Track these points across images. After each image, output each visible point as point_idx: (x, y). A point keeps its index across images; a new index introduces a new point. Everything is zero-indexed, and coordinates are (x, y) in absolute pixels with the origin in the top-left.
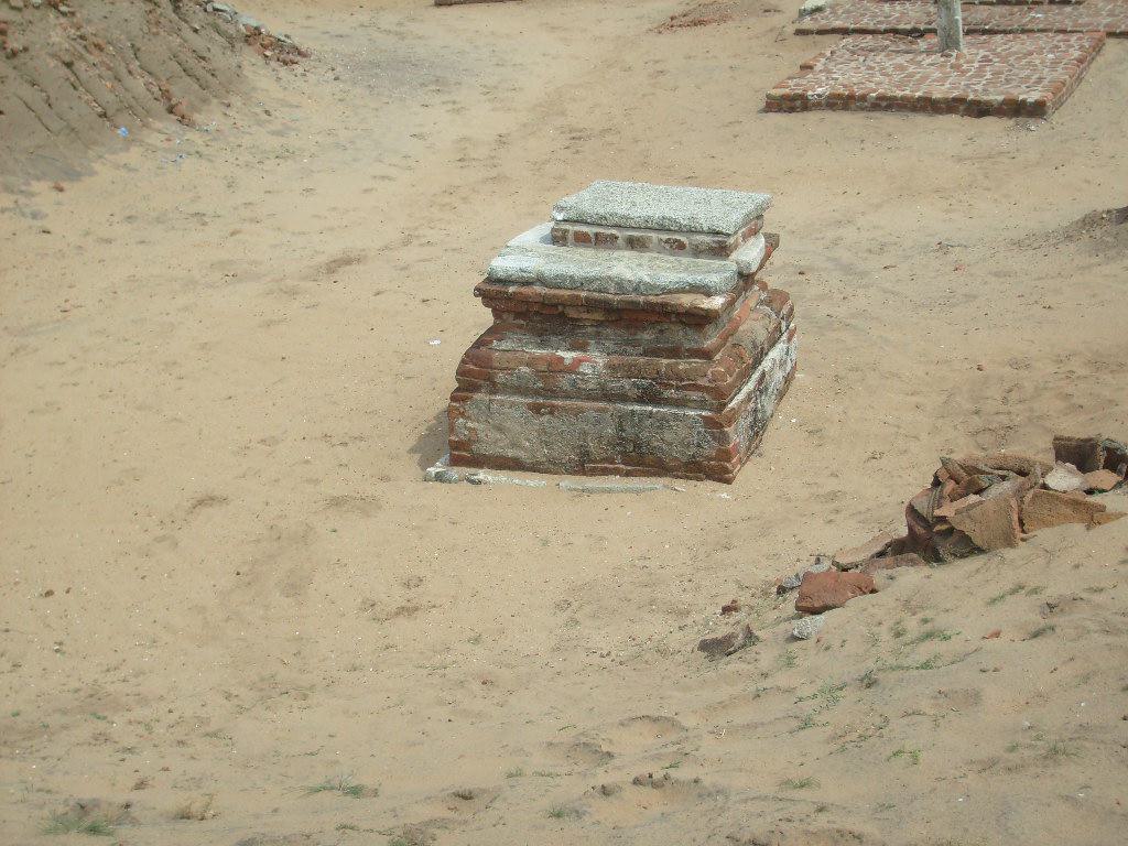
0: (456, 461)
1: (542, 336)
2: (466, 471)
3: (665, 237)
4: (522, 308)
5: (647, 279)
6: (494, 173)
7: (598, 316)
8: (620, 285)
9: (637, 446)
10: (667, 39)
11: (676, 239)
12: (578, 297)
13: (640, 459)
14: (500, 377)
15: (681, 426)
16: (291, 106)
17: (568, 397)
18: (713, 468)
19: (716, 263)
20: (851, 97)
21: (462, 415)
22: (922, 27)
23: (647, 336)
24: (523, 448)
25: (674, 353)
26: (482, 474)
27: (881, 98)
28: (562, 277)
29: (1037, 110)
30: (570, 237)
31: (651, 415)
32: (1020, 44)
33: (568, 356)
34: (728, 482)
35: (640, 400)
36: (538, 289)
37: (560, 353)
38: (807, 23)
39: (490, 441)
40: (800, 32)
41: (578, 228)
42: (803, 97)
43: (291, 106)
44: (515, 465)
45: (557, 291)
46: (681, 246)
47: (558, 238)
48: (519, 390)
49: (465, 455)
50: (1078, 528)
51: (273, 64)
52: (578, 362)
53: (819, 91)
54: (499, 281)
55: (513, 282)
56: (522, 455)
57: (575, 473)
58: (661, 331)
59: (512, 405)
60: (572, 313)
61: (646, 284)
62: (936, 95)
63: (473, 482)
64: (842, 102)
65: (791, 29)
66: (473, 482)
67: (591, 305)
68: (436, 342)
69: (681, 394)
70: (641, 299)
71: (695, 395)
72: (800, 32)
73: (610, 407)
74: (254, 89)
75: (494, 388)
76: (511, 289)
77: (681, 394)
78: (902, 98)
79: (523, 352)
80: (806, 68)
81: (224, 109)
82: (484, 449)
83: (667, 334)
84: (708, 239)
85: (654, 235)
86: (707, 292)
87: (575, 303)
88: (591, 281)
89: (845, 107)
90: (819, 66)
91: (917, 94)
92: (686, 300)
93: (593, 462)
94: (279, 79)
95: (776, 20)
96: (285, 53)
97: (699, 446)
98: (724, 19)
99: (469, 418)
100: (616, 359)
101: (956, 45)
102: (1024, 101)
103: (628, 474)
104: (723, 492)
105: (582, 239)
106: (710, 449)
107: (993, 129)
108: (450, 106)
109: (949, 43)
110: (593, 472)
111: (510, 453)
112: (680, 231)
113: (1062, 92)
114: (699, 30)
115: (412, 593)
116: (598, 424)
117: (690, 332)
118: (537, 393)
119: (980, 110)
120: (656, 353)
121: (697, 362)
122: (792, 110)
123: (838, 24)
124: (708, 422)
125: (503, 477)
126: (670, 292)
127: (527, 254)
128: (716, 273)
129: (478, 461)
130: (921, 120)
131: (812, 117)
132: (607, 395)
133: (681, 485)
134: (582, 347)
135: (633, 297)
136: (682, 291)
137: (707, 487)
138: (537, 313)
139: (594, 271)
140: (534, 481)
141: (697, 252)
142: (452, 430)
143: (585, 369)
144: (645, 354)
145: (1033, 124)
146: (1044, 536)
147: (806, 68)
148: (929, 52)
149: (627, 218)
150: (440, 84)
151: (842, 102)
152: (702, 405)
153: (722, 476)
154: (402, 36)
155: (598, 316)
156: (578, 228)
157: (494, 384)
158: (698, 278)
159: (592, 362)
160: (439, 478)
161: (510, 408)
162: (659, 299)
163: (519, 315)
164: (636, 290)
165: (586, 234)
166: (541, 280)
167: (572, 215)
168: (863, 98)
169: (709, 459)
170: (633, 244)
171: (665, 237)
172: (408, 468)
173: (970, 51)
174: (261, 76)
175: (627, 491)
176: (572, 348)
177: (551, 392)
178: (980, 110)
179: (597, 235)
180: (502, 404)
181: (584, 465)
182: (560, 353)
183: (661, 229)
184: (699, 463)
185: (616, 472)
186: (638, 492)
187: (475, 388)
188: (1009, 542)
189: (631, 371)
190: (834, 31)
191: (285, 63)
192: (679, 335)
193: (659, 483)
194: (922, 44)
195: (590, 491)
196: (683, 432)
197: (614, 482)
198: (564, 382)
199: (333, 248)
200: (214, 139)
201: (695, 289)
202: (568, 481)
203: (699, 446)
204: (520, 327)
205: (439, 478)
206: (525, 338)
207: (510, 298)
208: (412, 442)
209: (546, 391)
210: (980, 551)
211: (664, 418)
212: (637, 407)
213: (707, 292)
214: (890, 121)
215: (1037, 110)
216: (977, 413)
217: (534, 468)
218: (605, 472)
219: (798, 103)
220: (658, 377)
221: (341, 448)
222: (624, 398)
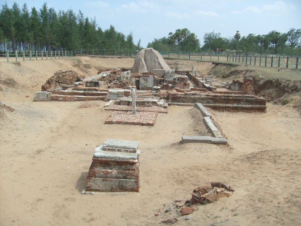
0: (87, 190)
1: (104, 167)
2: (90, 192)
3: (125, 149)
4: (97, 162)
5: (124, 157)
6: (59, 134)
7: (115, 164)
8: (119, 158)
9: (122, 186)
10: (80, 110)
11: (127, 150)
12: (112, 160)
13: (122, 189)
14: (97, 175)
15: (130, 182)
16: (15, 120)
17: (109, 178)
18: (135, 189)
19: (134, 154)
20: (120, 122)
21: (89, 182)
22: (127, 110)
23: (123, 167)
24: (101, 188)
25: (129, 170)
26: (93, 193)
27: (126, 122)
28: (109, 157)
29: (152, 125)
30: (107, 149)
31: (125, 181)
32: (145, 113)
33: (110, 171)
34: (138, 192)
35: (123, 178)
36: (104, 159)
37: (108, 170)
38: (106, 108)
39: (94, 187)
40: (105, 110)
41: (108, 148)
42: (112, 122)
43: (15, 120)
44: (99, 191)
45: (108, 159)
46: (127, 151)
47: (104, 149)
48: (100, 177)
49: (89, 189)
50: (226, 197)
51: (9, 111)
52: (112, 172)
53: (115, 121)
54: (97, 157)
55: (100, 158)
56: (100, 189)
57: (110, 192)
58: (126, 166)
59: (99, 180)
60: (110, 163)
61: (124, 158)
62: (135, 122)
63: (91, 194)
64: (119, 123)
65: (104, 109)
66: (91, 194)
67: (114, 162)
68: (69, 167)
69: (131, 177)
70: (123, 160)
71: (133, 177)
72: (105, 110)
73: (117, 179)
74: (7, 116)
75: (95, 177)
76: (99, 159)
77: (131, 177)
78: (129, 122)
79: (100, 170)
80: (110, 116)
81: (3, 120)
82: (92, 188)
83: (127, 167)
84: (132, 150)
85: (122, 149)
86: (134, 159)
87: (111, 161)
88: (114, 157)
89: (119, 124)
90: (112, 116)
91: (132, 122)
92: (131, 160)
93: (114, 189)
94: (11, 114)
95: (99, 107)
96: (11, 110)
97: (134, 186)
98: (90, 107)
99: (90, 182)
100: (119, 171)
101: (135, 113)
102: (150, 123)
103: (120, 191)
104: (138, 194)
105: (109, 150)
106: (135, 187)
107: (145, 127)
108: (45, 121)
109: (134, 113)
110: (114, 191)
111: (98, 188)
112: (127, 148)
113: (155, 121)
114: (86, 108)
115: (91, 216)
116: (115, 183)
117: (131, 166)
118: (104, 177)
119: (143, 125)
120: (126, 170)
121: (133, 171)
122: (110, 124)
123: (112, 109)
124: (135, 182)
125: (97, 193)
126: (128, 159)
127: (99, 153)
128: (134, 156)
129: (91, 190)
130: (133, 126)
131: (114, 125)
132: (117, 177)
133: (130, 193)
134: (112, 169)
135: (121, 160)
136: (130, 159)
137: (135, 193)
138: (104, 163)
139: (114, 156)
140: (103, 193)
141: (130, 152)
142: (87, 184)
143: (113, 173)
144: (123, 170)
145: (152, 127)
146: (221, 199)
147: (110, 116)
148: (130, 114)
149: (118, 146)
150: (42, 117)
151: (119, 123)
152: (134, 179)
153: (137, 191)
154: (31, 107)
155: (115, 164)
156: (108, 148)
157: (96, 176)
158: (133, 157)
159: (114, 172)
160: (85, 194)
161: (99, 181)
162: (127, 160)
163: (100, 163)
164: (122, 159)
165: (110, 149)
166: (105, 157)
167: (107, 145)
168: (123, 122)
169: (135, 188)
170: (118, 150)
171: (125, 149)
172: (76, 192)
173: (138, 114)
174: (7, 114)
175: (121, 194)
176: (110, 169)
177: (106, 177)
178: (143, 125)
179: (112, 149)
180: (97, 180)
181: (112, 190)
182: (108, 170)
183: (124, 148)
184: (133, 189)
185: (118, 191)
186: (123, 195)
187: (92, 177)
188: (216, 200)
189: (121, 173)
190: (111, 110)
191: (11, 111)
192: (129, 167)
193: (127, 193)
194: (128, 113)
195: (114, 195)
196: (131, 184)
197: (118, 193)
198: (109, 175)
199: (36, 148)
200: (3, 126)
201: (132, 159)
202: (109, 193)
203: (134, 186)
204: (100, 166)
205: (85, 194)
206: (101, 167)
207: (99, 160)
208: (75, 187)
209: (105, 177)
210: (212, 202)
211: (127, 181)
212: (122, 180)
213: (134, 159)
214: (128, 126)
215: (152, 125)
216: (174, 178)
217: (102, 191)
218: (116, 191)
219: (111, 123)
220: (126, 174)
221: (61, 189)
222: (120, 178)
